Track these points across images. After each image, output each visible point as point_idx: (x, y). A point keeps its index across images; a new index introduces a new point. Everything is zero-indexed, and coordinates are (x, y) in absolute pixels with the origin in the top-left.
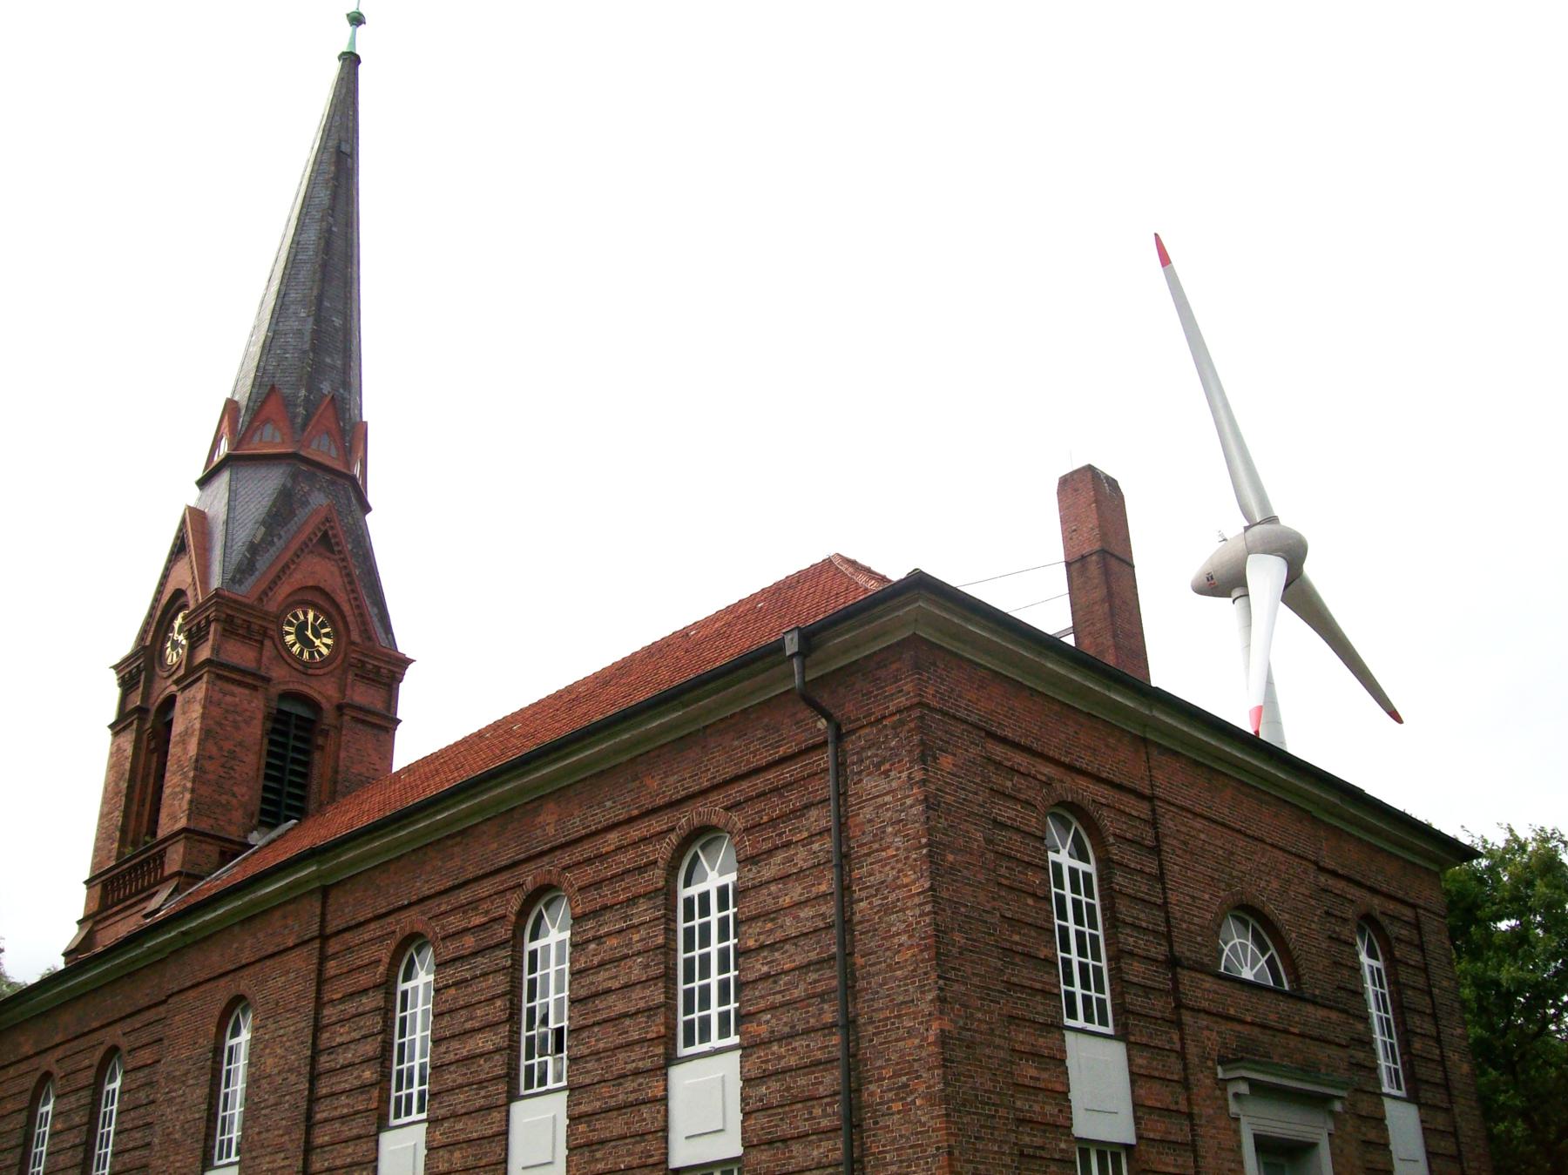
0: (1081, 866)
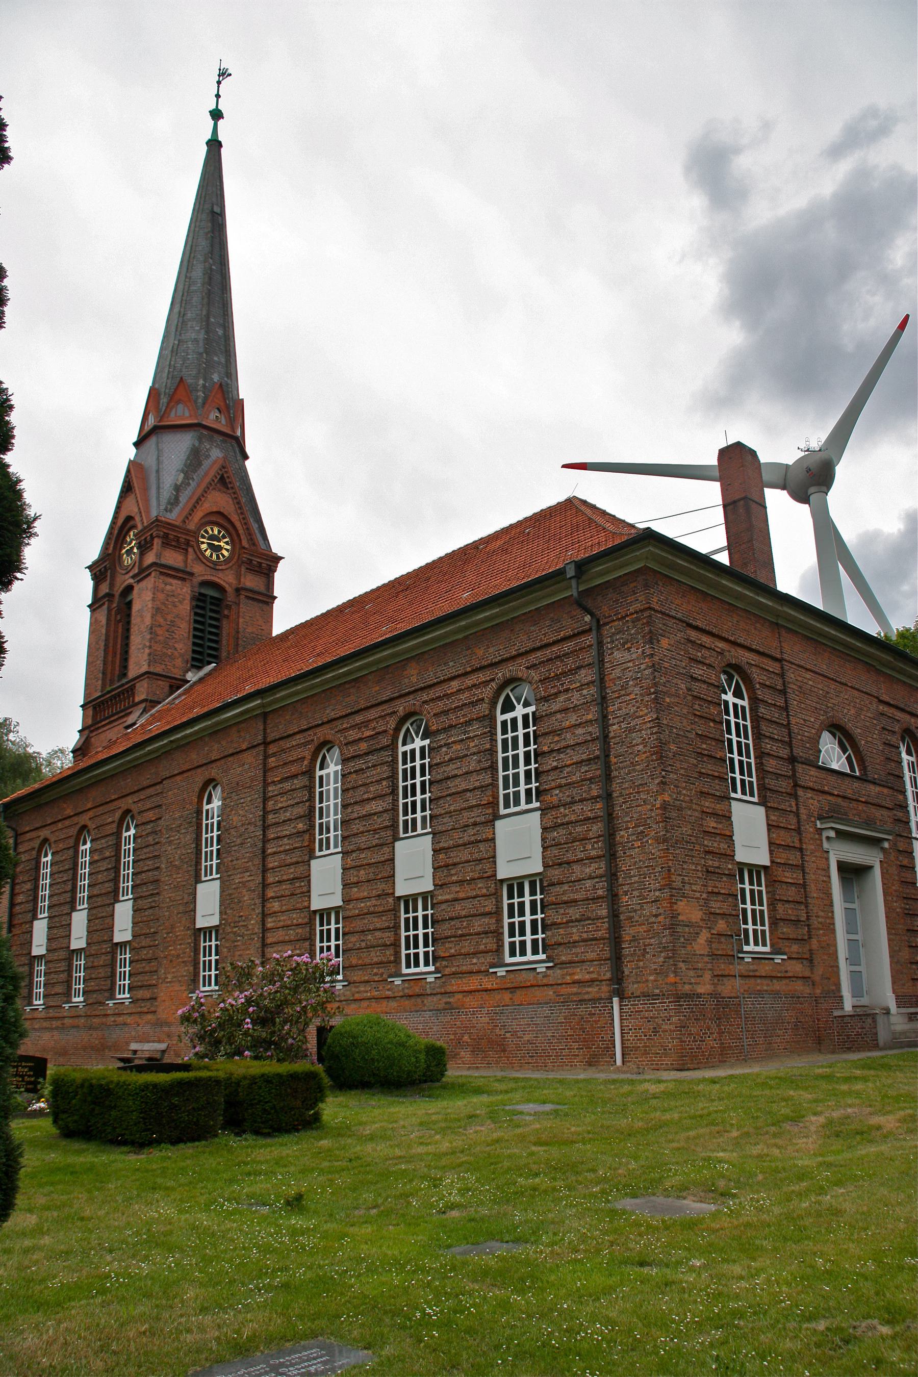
0: (739, 702)
